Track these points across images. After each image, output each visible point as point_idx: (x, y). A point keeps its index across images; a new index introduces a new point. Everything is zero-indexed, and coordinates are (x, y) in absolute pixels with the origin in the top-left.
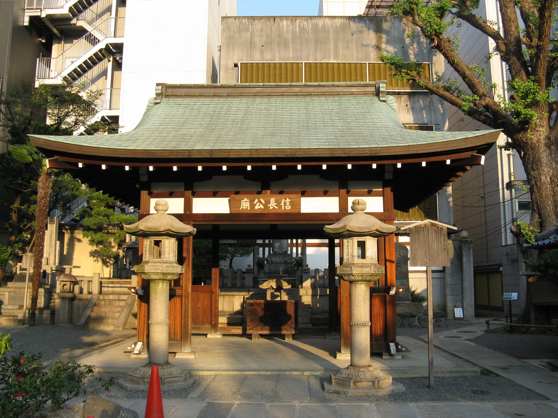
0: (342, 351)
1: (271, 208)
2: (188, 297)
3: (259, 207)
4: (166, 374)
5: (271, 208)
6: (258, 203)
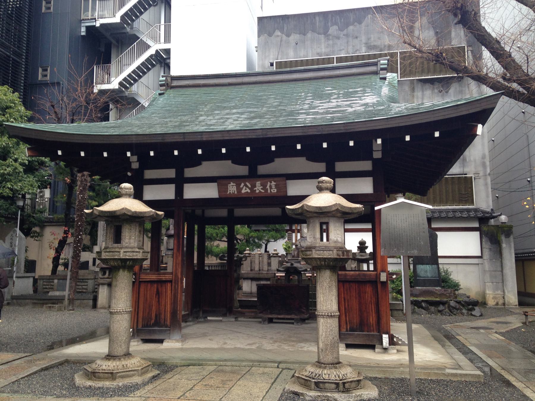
1: (257, 191)
2: (178, 282)
3: (246, 191)
5: (257, 191)
6: (245, 187)
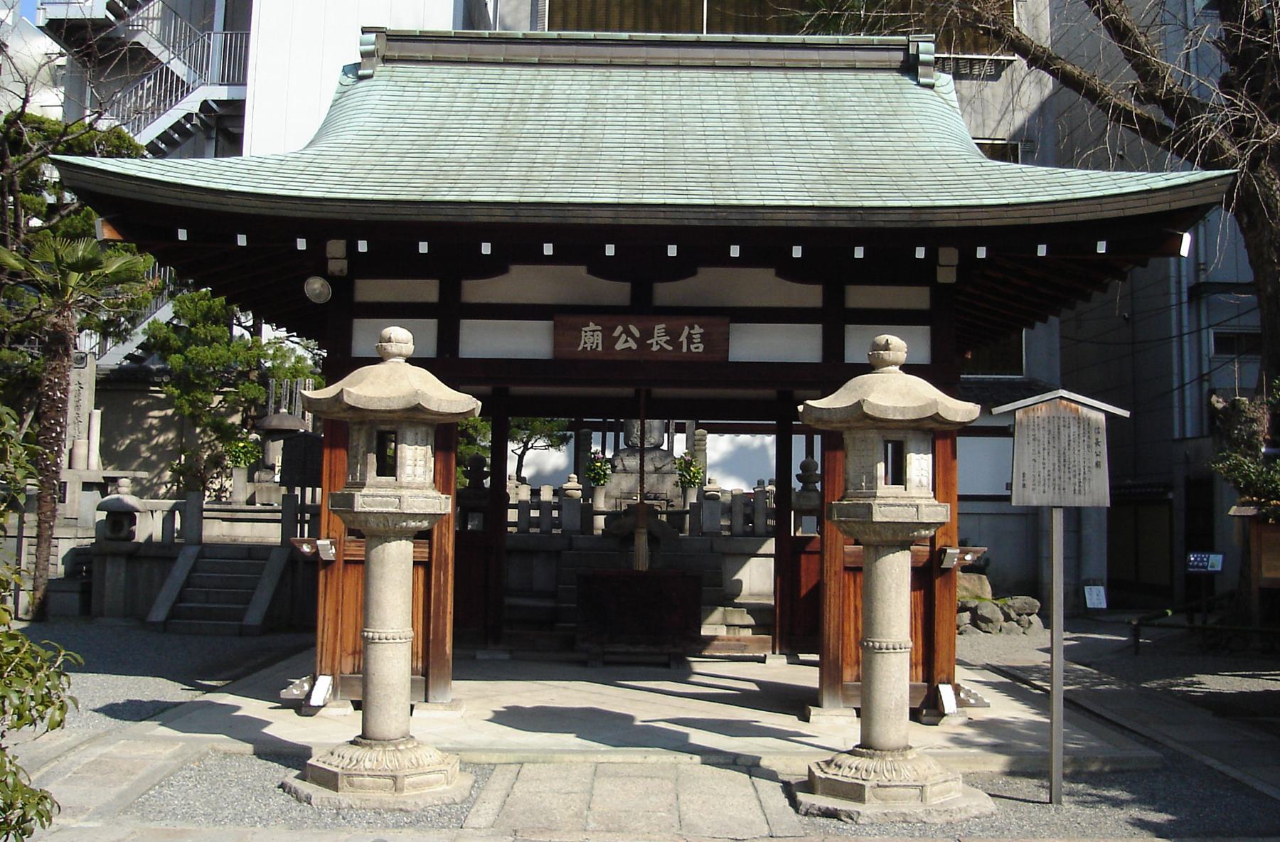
0: (825, 703)
1: (655, 348)
2: (447, 564)
3: (627, 345)
4: (407, 763)
5: (655, 348)
6: (624, 336)
